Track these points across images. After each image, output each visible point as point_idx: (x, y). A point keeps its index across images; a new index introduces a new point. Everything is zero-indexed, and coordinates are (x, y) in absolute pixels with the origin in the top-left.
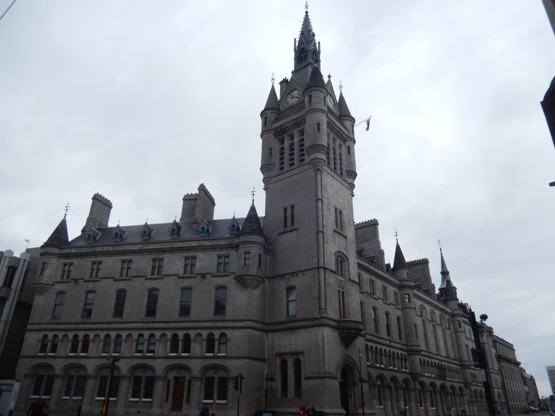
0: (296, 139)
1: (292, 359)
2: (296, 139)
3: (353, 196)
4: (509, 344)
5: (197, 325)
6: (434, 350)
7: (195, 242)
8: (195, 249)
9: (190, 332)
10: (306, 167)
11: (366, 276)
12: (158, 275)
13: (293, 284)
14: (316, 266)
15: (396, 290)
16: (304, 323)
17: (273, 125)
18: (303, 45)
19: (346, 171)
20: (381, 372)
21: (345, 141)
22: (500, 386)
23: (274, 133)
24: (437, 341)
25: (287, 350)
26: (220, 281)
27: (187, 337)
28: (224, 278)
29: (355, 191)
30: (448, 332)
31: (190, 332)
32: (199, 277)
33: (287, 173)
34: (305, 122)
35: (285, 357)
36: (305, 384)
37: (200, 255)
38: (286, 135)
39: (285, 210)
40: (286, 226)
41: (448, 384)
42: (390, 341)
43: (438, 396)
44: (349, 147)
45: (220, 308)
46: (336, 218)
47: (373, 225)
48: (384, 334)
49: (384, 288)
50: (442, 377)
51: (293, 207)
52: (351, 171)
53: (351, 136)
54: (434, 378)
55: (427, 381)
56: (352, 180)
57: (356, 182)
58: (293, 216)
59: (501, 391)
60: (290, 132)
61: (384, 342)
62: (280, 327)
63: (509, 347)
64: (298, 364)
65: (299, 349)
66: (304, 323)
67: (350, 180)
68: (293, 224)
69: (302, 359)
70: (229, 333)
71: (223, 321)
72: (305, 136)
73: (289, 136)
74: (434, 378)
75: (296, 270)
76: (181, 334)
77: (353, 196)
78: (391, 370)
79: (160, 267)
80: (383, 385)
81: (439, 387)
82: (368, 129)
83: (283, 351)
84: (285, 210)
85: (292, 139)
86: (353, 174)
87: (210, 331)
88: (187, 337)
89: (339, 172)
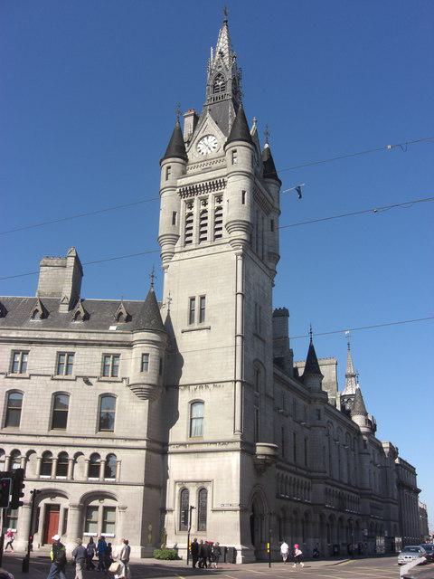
0: (210, 207)
1: (196, 488)
2: (210, 207)
3: (273, 286)
4: (410, 465)
5: (77, 441)
6: (291, 459)
7: (75, 334)
8: (74, 343)
9: (67, 450)
10: (225, 248)
11: (279, 388)
12: (66, 374)
13: (200, 398)
14: (233, 378)
15: (306, 404)
16: (213, 447)
17: (179, 181)
18: (220, 69)
19: (269, 253)
20: (285, 503)
21: (268, 213)
22: (397, 519)
23: (180, 192)
24: (372, 480)
25: (190, 478)
26: (108, 388)
27: (63, 456)
28: (113, 384)
29: (276, 279)
30: (352, 453)
31: (67, 450)
32: (80, 381)
33: (196, 251)
34: (225, 185)
35: (187, 485)
36: (210, 516)
37: (80, 352)
38: (196, 197)
39: (193, 299)
40: (191, 321)
41: (347, 517)
42: (297, 467)
43: (345, 530)
44: (272, 221)
45: (105, 422)
46: (256, 316)
47: (283, 314)
48: (291, 459)
49: (295, 404)
50: (341, 509)
51: (203, 298)
52: (274, 254)
53: (276, 206)
54: (334, 510)
55: (327, 513)
56: (273, 265)
57: (278, 268)
58: (202, 310)
59: (398, 524)
60: (202, 195)
61: (289, 467)
62: (182, 449)
63: (411, 472)
64: (202, 492)
65: (205, 478)
66: (213, 447)
67: (271, 265)
68: (201, 319)
69: (209, 489)
70: (120, 454)
71: (113, 439)
72: (224, 204)
73: (201, 199)
74: (334, 510)
75: (205, 381)
76: (55, 452)
77: (273, 286)
78: (295, 501)
79: (69, 365)
80: (285, 518)
81: (327, 517)
82: (300, 197)
83: (184, 478)
84: (193, 299)
85: (205, 204)
86: (275, 257)
87: (95, 450)
88: (63, 456)
89: (260, 255)
